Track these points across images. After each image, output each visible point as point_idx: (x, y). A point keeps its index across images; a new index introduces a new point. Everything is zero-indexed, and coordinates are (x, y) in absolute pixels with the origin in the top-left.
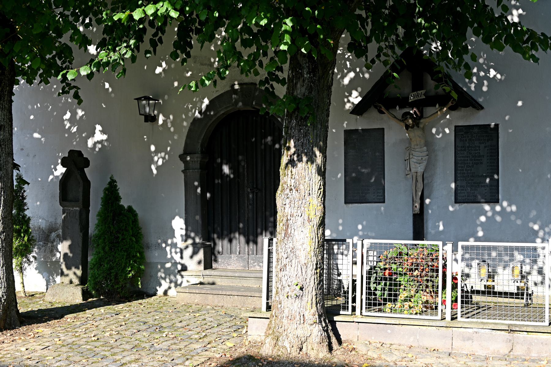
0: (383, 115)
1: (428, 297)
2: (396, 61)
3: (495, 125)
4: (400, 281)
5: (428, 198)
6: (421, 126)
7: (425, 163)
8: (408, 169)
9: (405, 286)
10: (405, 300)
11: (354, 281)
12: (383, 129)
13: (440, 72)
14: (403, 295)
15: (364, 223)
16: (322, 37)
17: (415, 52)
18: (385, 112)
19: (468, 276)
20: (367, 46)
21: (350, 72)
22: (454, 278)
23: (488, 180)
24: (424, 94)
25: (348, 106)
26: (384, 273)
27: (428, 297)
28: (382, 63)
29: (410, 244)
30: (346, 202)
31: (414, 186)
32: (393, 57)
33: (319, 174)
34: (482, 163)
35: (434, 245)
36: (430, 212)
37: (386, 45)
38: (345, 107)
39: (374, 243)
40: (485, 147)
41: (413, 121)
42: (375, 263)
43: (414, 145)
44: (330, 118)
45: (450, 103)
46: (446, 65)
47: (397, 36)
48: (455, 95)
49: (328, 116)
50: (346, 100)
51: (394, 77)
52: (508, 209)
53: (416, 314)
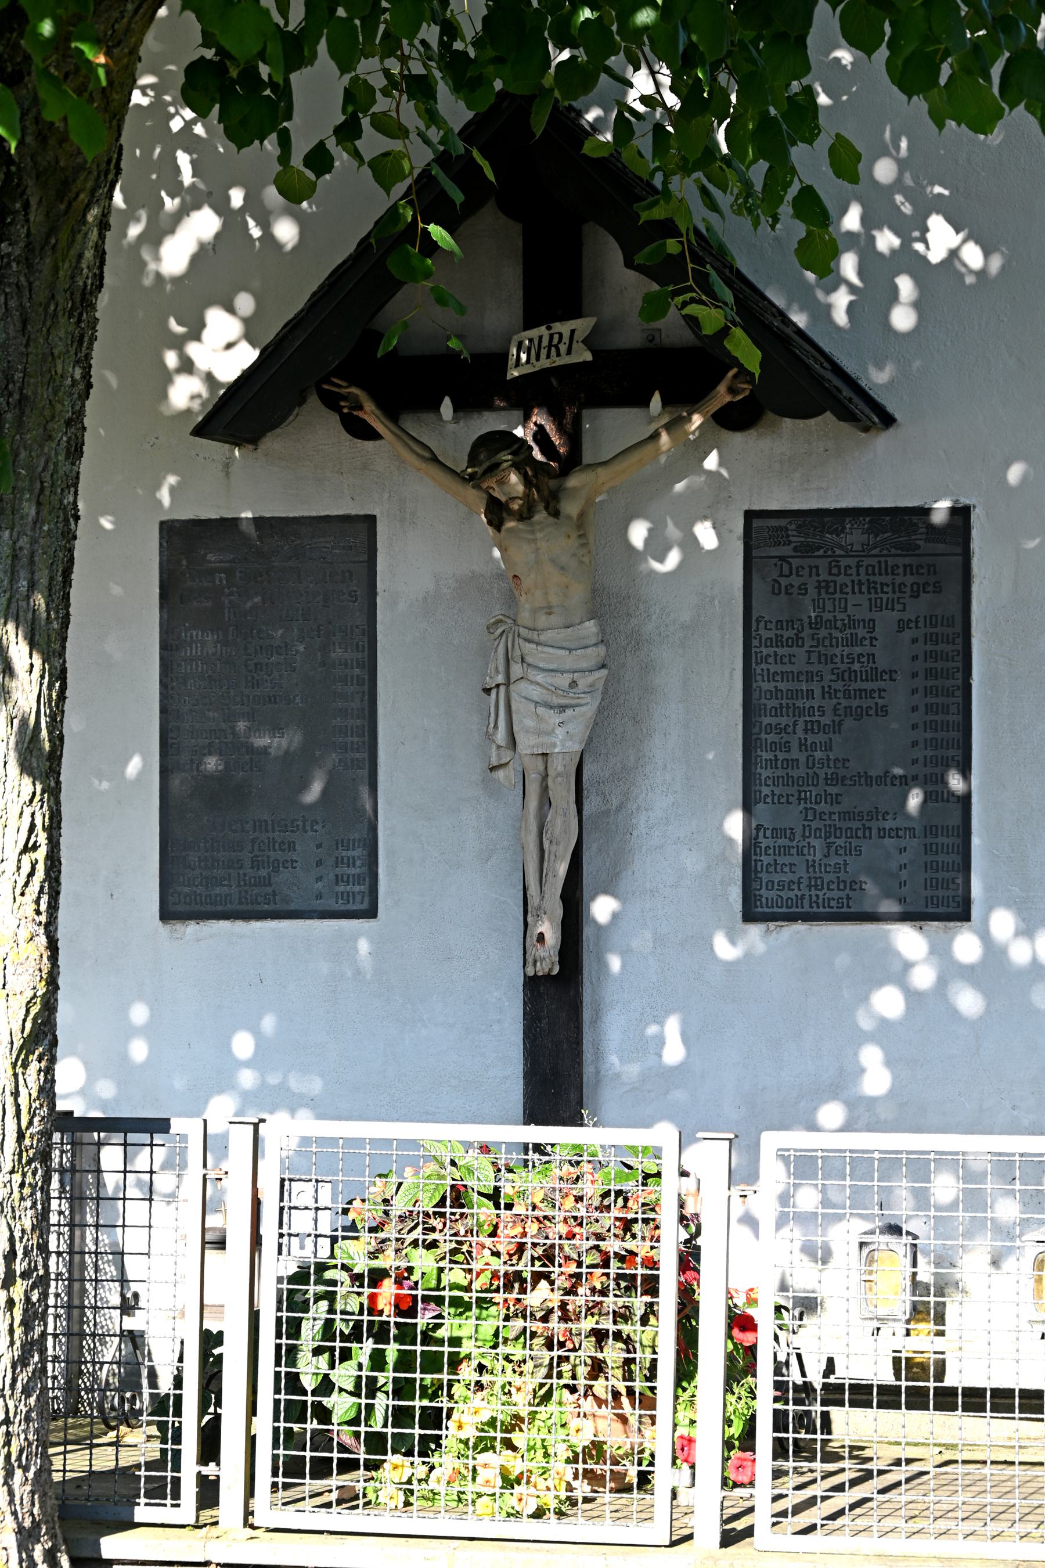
0: (369, 445)
1: (602, 1425)
2: (443, 159)
3: (954, 511)
4: (456, 1341)
5: (606, 892)
6: (570, 508)
7: (589, 708)
8: (501, 736)
9: (481, 1368)
10: (484, 1445)
11: (210, 1340)
12: (371, 520)
13: (668, 228)
14: (468, 1414)
15: (268, 1023)
16: (47, 28)
17: (539, 124)
18: (378, 426)
19: (808, 1306)
20: (287, 81)
21: (198, 207)
22: (740, 1322)
23: (914, 800)
25: (184, 393)
26: (373, 1298)
27: (602, 1425)
28: (366, 170)
29: (510, 1146)
30: (167, 915)
31: (533, 828)
32: (427, 142)
33: (25, 768)
35: (633, 1150)
36: (615, 963)
37: (387, 73)
38: (165, 396)
39: (320, 1141)
40: (902, 626)
41: (527, 482)
42: (325, 1244)
43: (535, 611)
44: (86, 466)
45: (722, 388)
46: (704, 191)
47: (450, 30)
48: (746, 352)
49: (76, 451)
50: (171, 359)
51: (430, 247)
52: (1020, 953)
53: (538, 1514)
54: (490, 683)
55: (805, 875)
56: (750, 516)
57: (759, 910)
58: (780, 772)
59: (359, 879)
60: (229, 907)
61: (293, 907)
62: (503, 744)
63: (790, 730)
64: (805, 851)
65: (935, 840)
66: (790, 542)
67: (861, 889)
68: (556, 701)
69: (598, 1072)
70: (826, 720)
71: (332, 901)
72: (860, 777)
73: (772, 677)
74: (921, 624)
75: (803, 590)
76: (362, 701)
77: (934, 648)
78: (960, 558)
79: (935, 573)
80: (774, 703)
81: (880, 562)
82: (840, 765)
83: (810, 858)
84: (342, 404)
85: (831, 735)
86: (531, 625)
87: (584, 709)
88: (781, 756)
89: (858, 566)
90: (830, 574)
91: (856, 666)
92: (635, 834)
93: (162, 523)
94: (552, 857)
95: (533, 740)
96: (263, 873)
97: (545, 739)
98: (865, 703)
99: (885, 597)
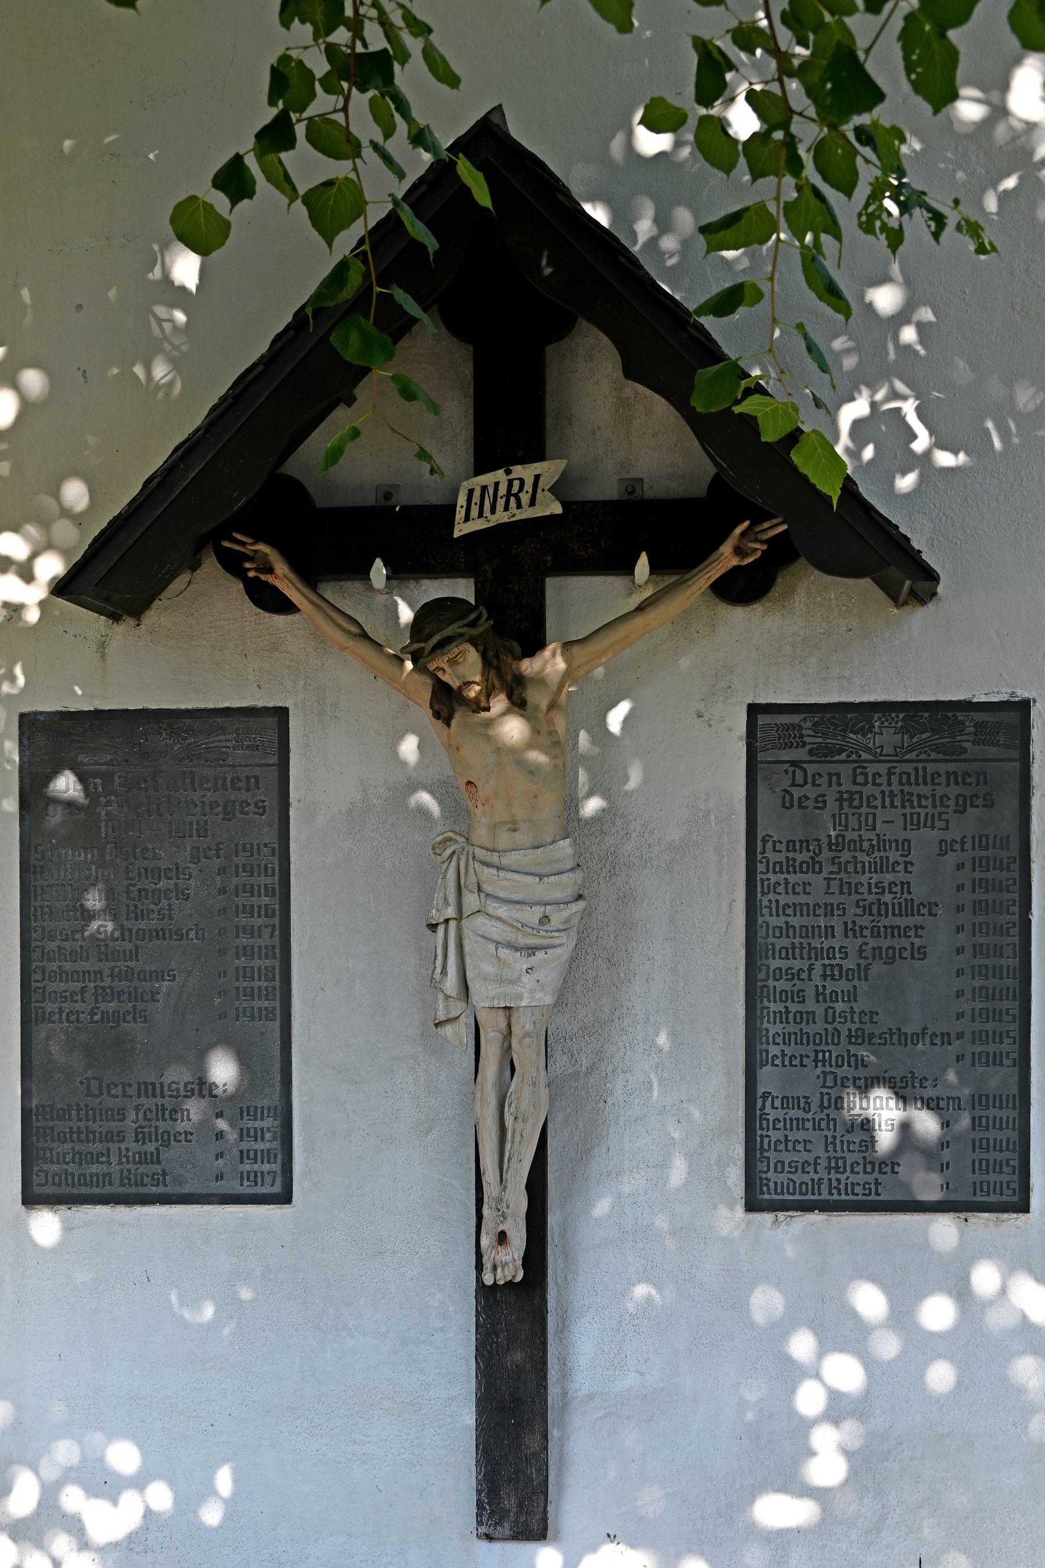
0: (280, 620)
7: (566, 944)
8: (451, 983)
12: (282, 714)
18: (293, 591)
24: (555, 490)
28: (300, 209)
34: (921, 953)
40: (944, 848)
43: (494, 827)
45: (726, 549)
54: (436, 917)
55: (823, 1155)
56: (754, 710)
57: (766, 1197)
58: (791, 1028)
59: (268, 1156)
60: (108, 1189)
61: (187, 1189)
62: (454, 994)
63: (804, 975)
64: (824, 1125)
65: (986, 1113)
66: (804, 744)
67: (893, 1171)
68: (523, 940)
69: (565, 1393)
70: (849, 964)
71: (236, 1183)
72: (891, 1034)
73: (781, 910)
74: (968, 845)
75: (821, 802)
76: (271, 937)
77: (984, 875)
78: (1017, 764)
79: (985, 783)
80: (786, 942)
81: (916, 769)
82: (866, 1019)
83: (829, 1134)
84: (247, 565)
85: (855, 982)
86: (489, 845)
87: (558, 951)
88: (793, 1007)
89: (890, 774)
90: (855, 783)
91: (887, 898)
92: (610, 1102)
93: (22, 716)
94: (518, 1138)
95: (492, 990)
96: (150, 1147)
97: (509, 989)
98: (898, 943)
99: (922, 812)
